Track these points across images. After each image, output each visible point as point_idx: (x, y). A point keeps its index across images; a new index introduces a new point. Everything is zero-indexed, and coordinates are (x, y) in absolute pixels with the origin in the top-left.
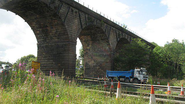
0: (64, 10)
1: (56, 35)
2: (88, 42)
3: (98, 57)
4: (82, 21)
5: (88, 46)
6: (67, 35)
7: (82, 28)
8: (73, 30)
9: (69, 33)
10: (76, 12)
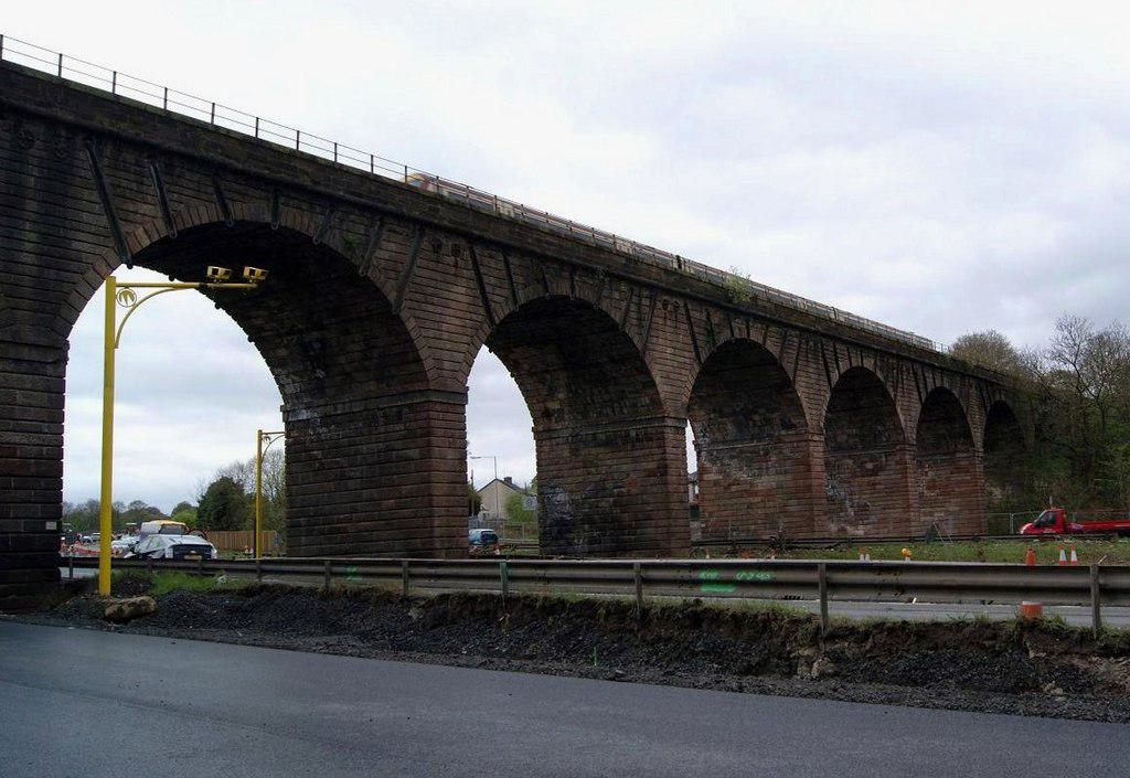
0: (393, 246)
1: (367, 363)
2: (548, 377)
3: (602, 450)
4: (488, 289)
5: (551, 394)
6: (418, 360)
7: (492, 322)
8: (445, 336)
9: (423, 353)
10: (456, 252)
